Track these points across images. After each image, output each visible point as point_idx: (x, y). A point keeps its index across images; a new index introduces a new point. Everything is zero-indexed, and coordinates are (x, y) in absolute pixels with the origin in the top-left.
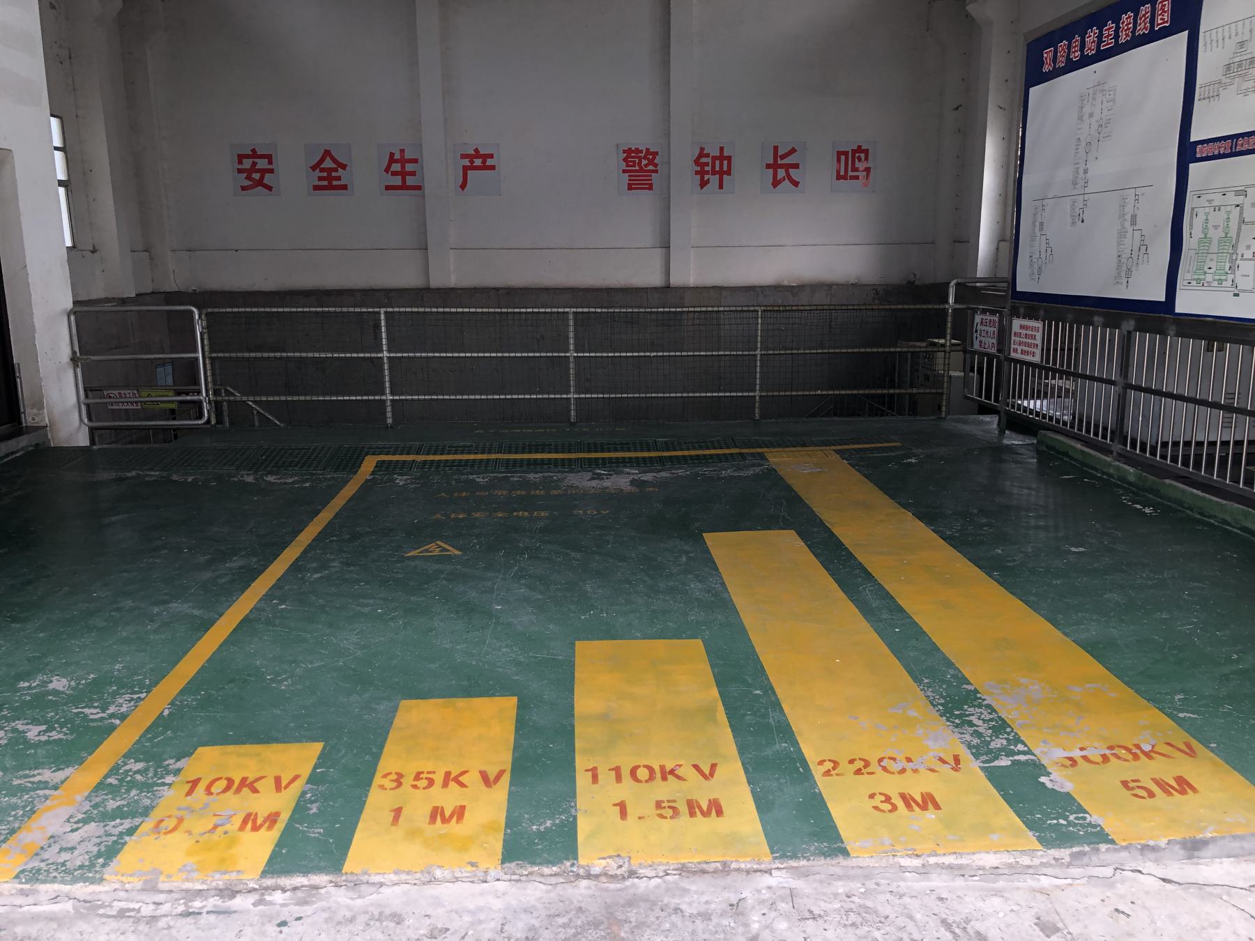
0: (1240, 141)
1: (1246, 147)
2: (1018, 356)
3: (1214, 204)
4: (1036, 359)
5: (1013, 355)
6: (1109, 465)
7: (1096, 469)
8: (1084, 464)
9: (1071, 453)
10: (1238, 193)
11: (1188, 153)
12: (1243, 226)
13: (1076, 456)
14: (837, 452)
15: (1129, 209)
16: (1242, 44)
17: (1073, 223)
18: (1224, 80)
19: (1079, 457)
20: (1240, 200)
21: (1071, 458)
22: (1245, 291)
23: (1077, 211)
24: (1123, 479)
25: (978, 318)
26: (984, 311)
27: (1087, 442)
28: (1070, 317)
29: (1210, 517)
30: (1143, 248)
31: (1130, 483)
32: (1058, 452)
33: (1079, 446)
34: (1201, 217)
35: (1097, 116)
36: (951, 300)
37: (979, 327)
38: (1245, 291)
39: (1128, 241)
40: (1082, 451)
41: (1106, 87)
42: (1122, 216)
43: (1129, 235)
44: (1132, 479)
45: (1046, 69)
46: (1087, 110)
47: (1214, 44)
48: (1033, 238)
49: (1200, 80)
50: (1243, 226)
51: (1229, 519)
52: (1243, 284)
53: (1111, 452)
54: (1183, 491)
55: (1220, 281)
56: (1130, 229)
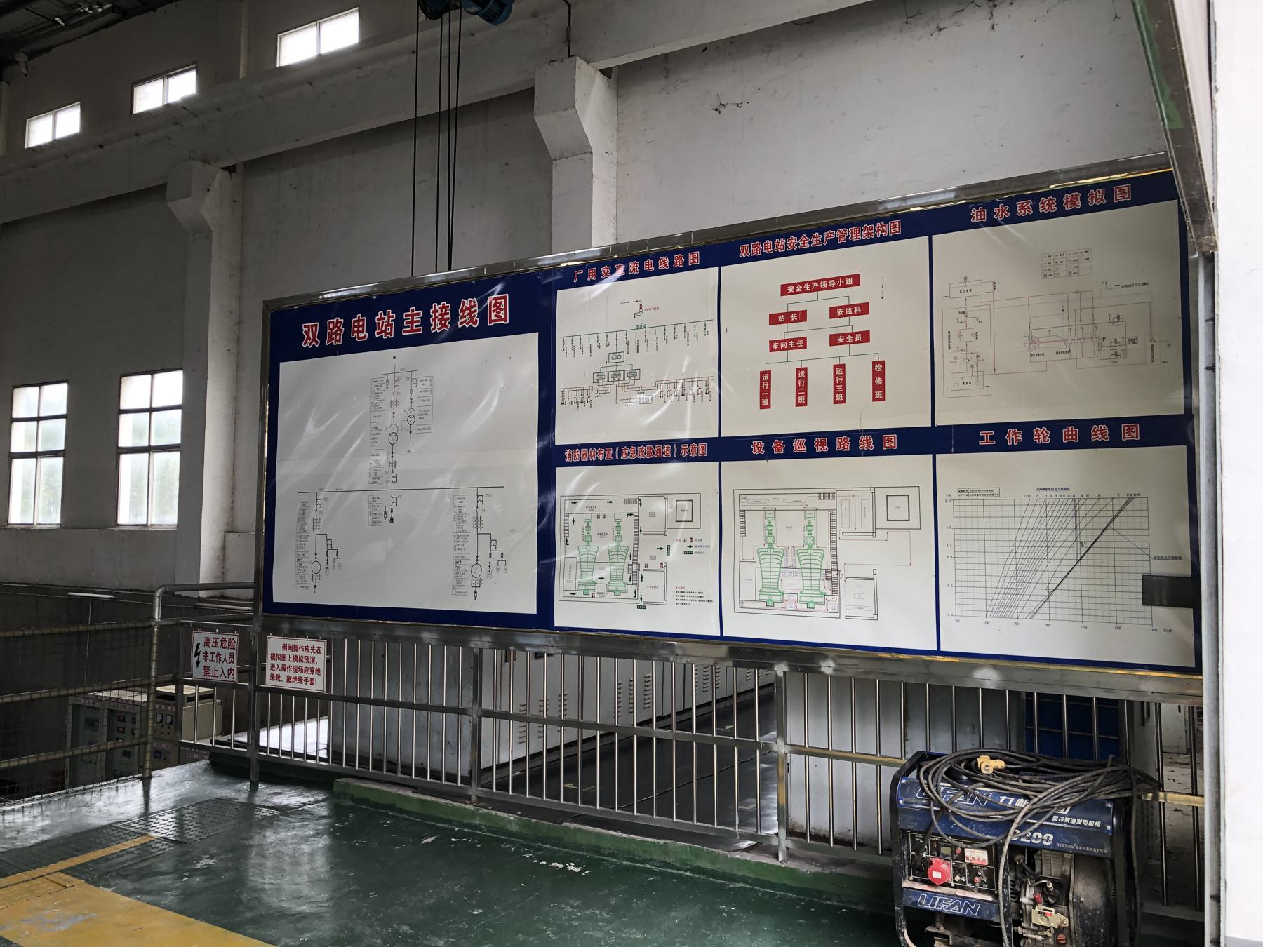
0: (625, 450)
1: (633, 456)
2: (283, 684)
3: (596, 511)
4: (320, 686)
5: (270, 683)
6: (473, 814)
7: (449, 822)
8: (423, 817)
9: (399, 805)
10: (628, 502)
11: (552, 459)
12: (641, 536)
13: (407, 807)
14: (69, 871)
15: (469, 511)
16: (616, 355)
17: (375, 523)
18: (596, 387)
19: (415, 808)
20: (634, 508)
21: (401, 811)
22: (652, 603)
23: (381, 509)
24: (500, 830)
25: (199, 638)
26: (205, 629)
27: (415, 789)
28: (378, 633)
29: (643, 862)
30: (332, 554)
31: (511, 834)
32: (376, 805)
33: (410, 793)
34: (581, 524)
35: (405, 404)
36: (157, 615)
37: (202, 649)
38: (652, 603)
39: (470, 547)
40: (421, 801)
41: (415, 375)
42: (459, 517)
43: (312, 538)
44: (514, 828)
45: (307, 344)
46: (387, 396)
47: (578, 351)
48: (301, 538)
49: (560, 384)
50: (641, 536)
51: (670, 860)
52: (647, 596)
53: (468, 797)
54: (600, 835)
55: (617, 593)
56: (473, 533)
